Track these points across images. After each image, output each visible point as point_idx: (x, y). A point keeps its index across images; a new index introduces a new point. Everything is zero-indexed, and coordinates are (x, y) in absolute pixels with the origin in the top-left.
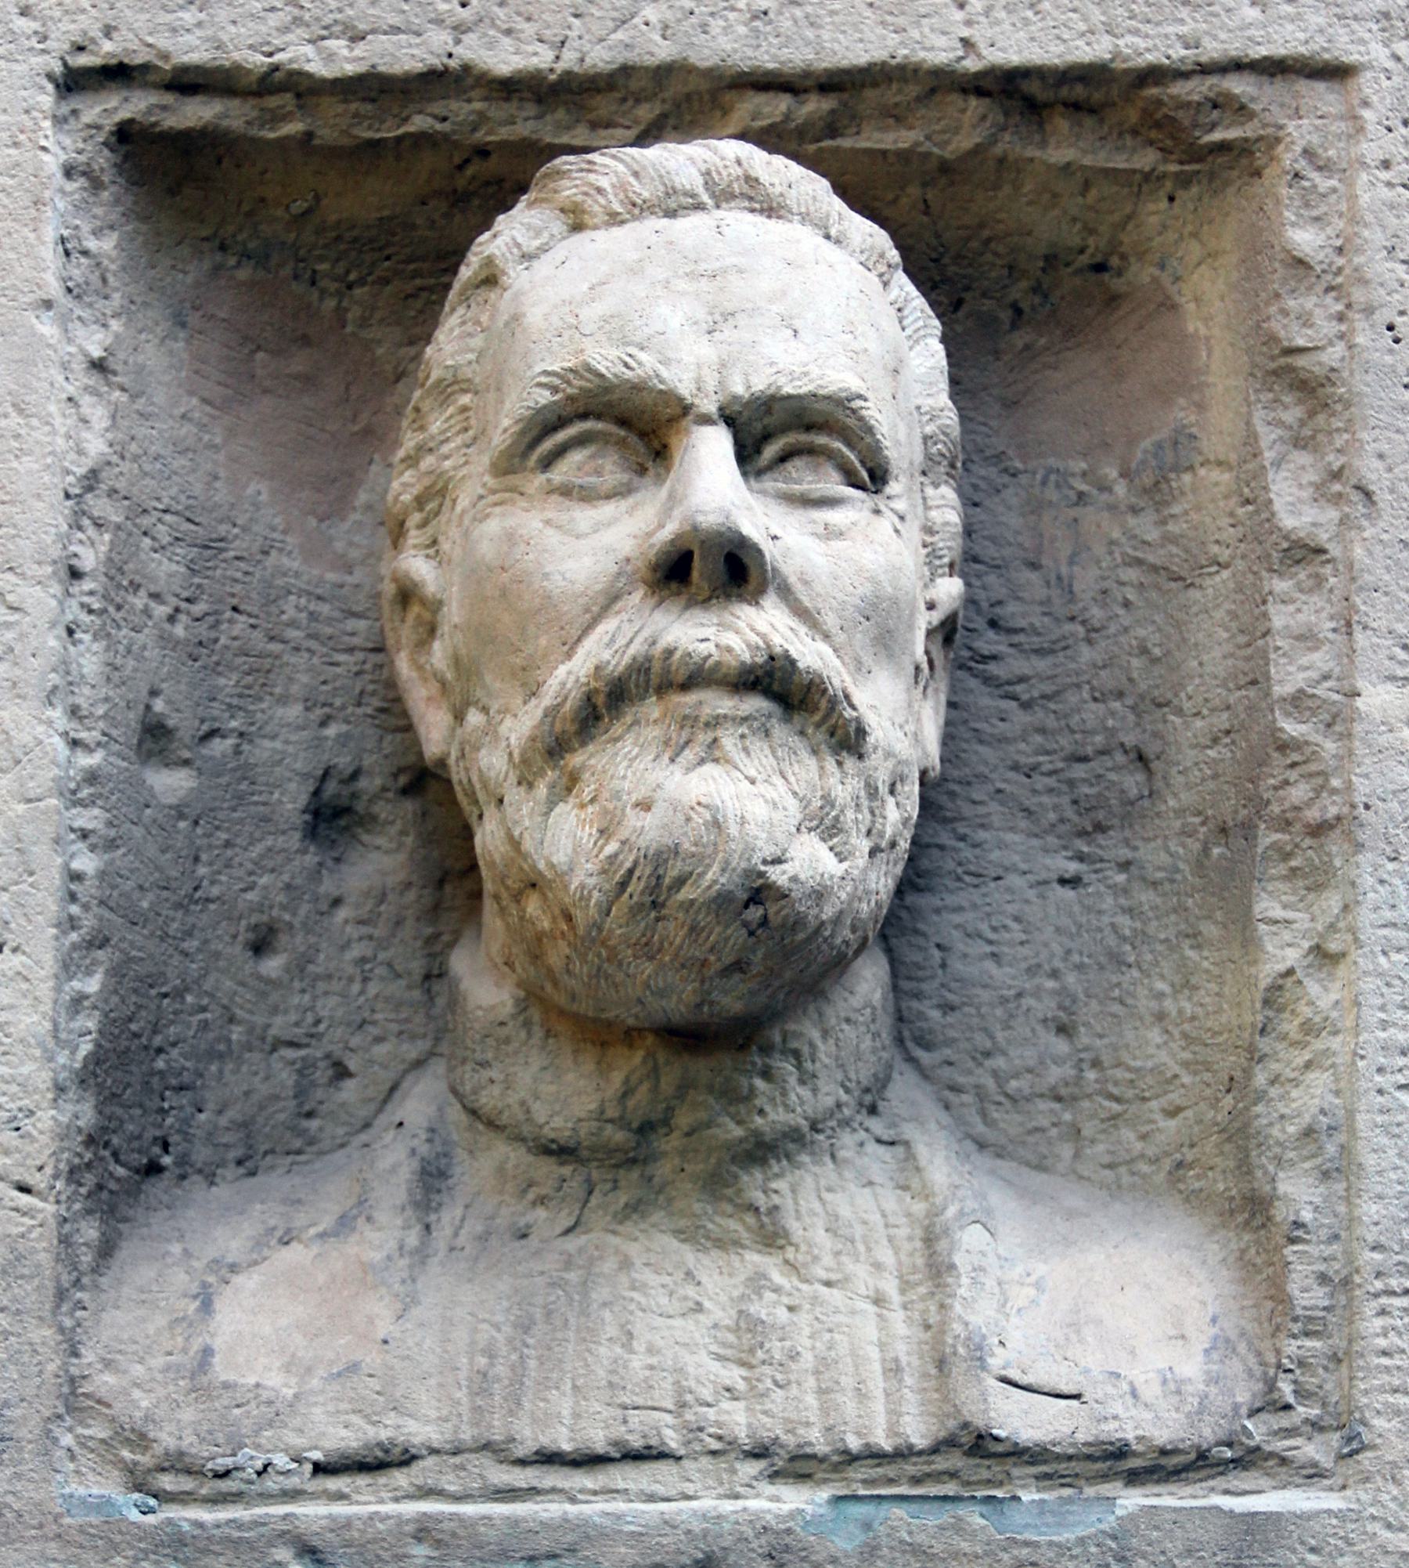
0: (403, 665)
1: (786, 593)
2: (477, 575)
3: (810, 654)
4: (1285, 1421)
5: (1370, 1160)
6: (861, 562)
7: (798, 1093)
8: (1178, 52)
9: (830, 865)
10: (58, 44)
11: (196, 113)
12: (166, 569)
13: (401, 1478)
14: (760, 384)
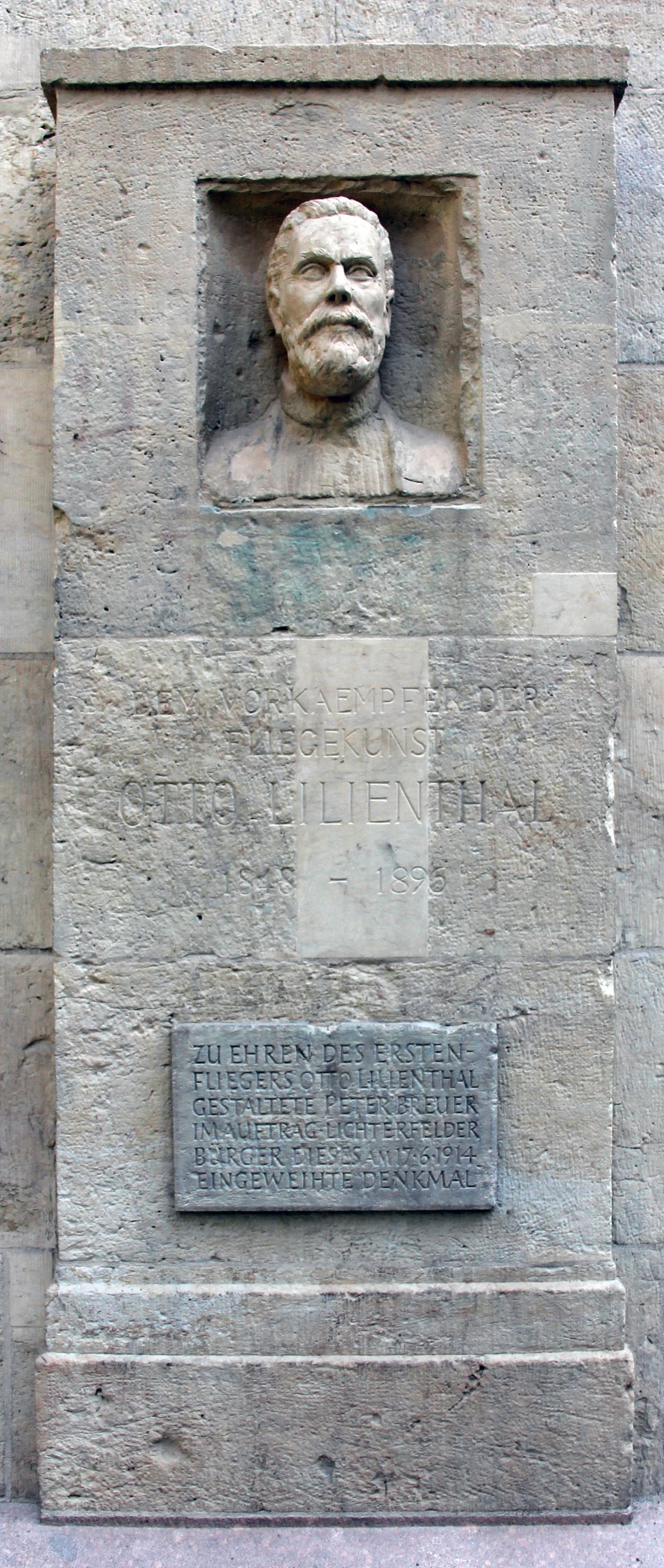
0: (271, 311)
1: (356, 302)
2: (288, 296)
3: (361, 316)
4: (467, 488)
5: (485, 427)
6: (373, 291)
7: (360, 411)
8: (439, 172)
9: (366, 363)
10: (196, 174)
11: (226, 188)
12: (218, 288)
13: (273, 503)
14: (349, 256)
